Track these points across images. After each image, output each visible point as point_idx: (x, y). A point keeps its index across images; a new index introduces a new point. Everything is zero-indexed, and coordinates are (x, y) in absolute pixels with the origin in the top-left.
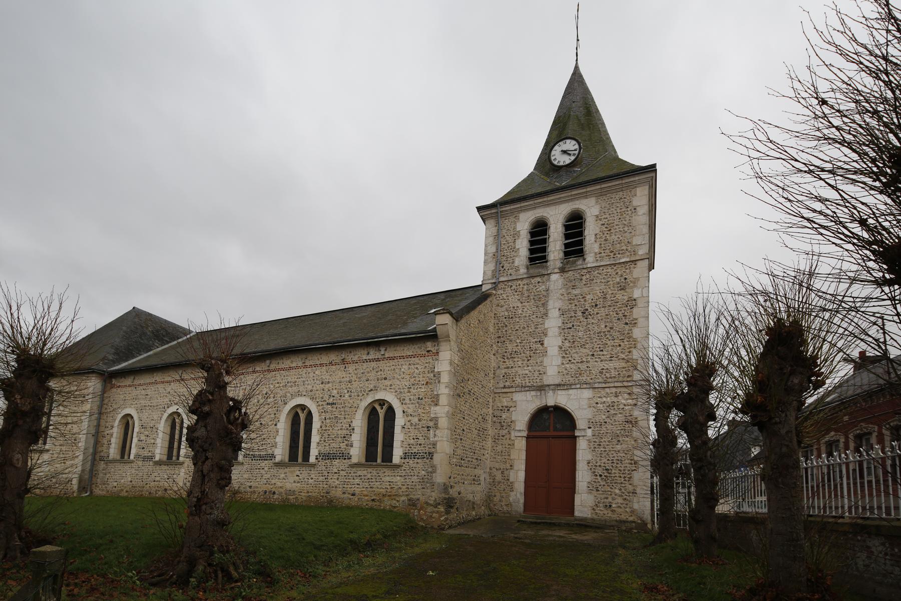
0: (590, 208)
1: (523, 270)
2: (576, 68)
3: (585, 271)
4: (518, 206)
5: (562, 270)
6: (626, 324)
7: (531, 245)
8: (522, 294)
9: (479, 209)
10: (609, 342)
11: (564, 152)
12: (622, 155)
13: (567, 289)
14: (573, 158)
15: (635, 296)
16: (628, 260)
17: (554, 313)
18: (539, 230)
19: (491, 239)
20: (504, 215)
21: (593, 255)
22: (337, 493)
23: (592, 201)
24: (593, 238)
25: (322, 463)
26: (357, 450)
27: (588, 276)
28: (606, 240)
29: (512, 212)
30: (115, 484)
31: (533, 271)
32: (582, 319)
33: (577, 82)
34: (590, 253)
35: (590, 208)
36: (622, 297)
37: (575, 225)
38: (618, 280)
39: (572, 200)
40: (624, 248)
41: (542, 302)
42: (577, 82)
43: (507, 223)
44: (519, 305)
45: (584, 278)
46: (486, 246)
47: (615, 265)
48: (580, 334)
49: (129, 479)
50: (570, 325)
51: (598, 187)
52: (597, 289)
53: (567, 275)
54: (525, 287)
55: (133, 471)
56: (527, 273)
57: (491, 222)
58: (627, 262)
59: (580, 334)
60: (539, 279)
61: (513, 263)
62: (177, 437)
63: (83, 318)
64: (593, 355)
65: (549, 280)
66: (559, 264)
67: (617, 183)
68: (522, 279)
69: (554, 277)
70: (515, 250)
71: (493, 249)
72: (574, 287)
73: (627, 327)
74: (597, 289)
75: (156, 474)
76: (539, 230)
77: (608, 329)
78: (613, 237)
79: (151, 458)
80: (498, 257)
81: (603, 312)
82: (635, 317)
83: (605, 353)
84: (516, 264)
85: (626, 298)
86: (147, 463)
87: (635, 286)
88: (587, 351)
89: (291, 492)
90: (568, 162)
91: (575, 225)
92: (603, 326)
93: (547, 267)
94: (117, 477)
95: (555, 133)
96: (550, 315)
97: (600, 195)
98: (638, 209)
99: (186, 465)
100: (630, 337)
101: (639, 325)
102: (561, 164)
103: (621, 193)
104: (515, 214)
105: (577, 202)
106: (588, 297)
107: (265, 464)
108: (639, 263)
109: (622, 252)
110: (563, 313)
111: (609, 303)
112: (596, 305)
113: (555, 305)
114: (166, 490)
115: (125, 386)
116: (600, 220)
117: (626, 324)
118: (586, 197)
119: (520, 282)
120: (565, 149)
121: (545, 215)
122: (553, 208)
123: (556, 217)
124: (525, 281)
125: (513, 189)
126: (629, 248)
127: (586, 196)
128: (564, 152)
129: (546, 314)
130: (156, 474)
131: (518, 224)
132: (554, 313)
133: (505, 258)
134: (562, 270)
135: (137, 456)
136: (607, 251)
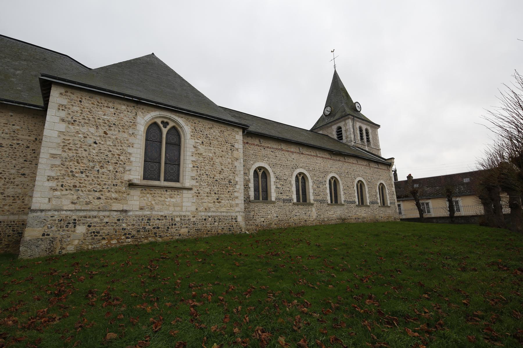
0: (341, 124)
12: (93, 67)
22: (377, 217)
25: (371, 205)
26: (188, 146)
30: (263, 219)
49: (275, 215)
55: (277, 210)
63: (97, 50)
75: (296, 211)
79: (290, 200)
86: (287, 204)
89: (364, 218)
94: (262, 214)
99: (315, 205)
107: (352, 205)
114: (306, 221)
115: (253, 144)
127: (341, 122)
130: (296, 211)
135: (278, 199)
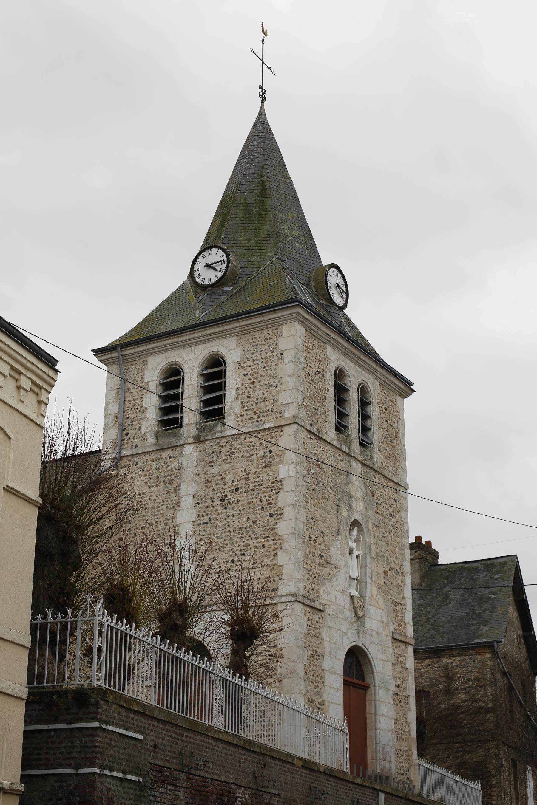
0: (231, 349)
1: (151, 440)
2: (262, 114)
3: (225, 440)
4: (144, 348)
5: (198, 440)
6: (271, 515)
7: (206, 381)
8: (151, 474)
9: (97, 352)
10: (251, 542)
11: (209, 266)
13: (204, 466)
14: (220, 275)
15: (281, 476)
16: (272, 425)
17: (187, 502)
18: (173, 378)
19: (113, 393)
20: (125, 360)
21: (233, 417)
23: (232, 342)
24: (234, 395)
27: (228, 448)
28: (249, 397)
29: (139, 355)
31: (164, 441)
32: (221, 510)
33: (261, 136)
34: (230, 415)
35: (231, 349)
36: (266, 477)
37: (214, 372)
38: (262, 453)
39: (209, 340)
40: (269, 408)
41: (172, 483)
42: (261, 136)
43: (133, 371)
44: (147, 490)
45: (223, 450)
46: (107, 404)
47: (258, 431)
48: (218, 531)
50: (206, 519)
51: (237, 325)
52: (239, 465)
53: (203, 446)
54: (154, 463)
56: (156, 444)
57: (115, 369)
58: (272, 428)
59: (218, 531)
60: (169, 452)
61: (140, 428)
62: (24, 361)
64: (233, 561)
65: (181, 453)
66: (194, 431)
67: (258, 320)
68: (150, 452)
69: (189, 449)
70: (142, 410)
71: (115, 409)
72: (211, 464)
73: (272, 520)
74: (239, 465)
76: (173, 378)
77: (251, 522)
78: (257, 392)
80: (122, 421)
81: (245, 498)
82: (280, 505)
83: (247, 557)
84: (143, 431)
85: (271, 478)
87: (281, 462)
88: (226, 555)
90: (214, 280)
91: (214, 372)
92: (244, 519)
93: (180, 435)
95: (219, 221)
96: (182, 505)
97: (242, 333)
98: (284, 354)
100: (275, 534)
101: (285, 516)
102: (206, 282)
103: (266, 331)
104: (142, 357)
105: (216, 343)
106: (228, 478)
108: (286, 429)
109: (267, 414)
110: (198, 500)
111: (252, 486)
112: (237, 490)
113: (189, 489)
116: (243, 368)
117: (271, 515)
118: (226, 336)
119: (147, 457)
120: (210, 262)
121: (178, 360)
122: (187, 350)
123: (191, 360)
124: (154, 456)
125: (151, 314)
126: (274, 408)
127: (225, 335)
128: (209, 266)
129: (178, 504)
131: (146, 373)
132: (187, 502)
133: (129, 422)
134: (198, 440)
136: (250, 412)
